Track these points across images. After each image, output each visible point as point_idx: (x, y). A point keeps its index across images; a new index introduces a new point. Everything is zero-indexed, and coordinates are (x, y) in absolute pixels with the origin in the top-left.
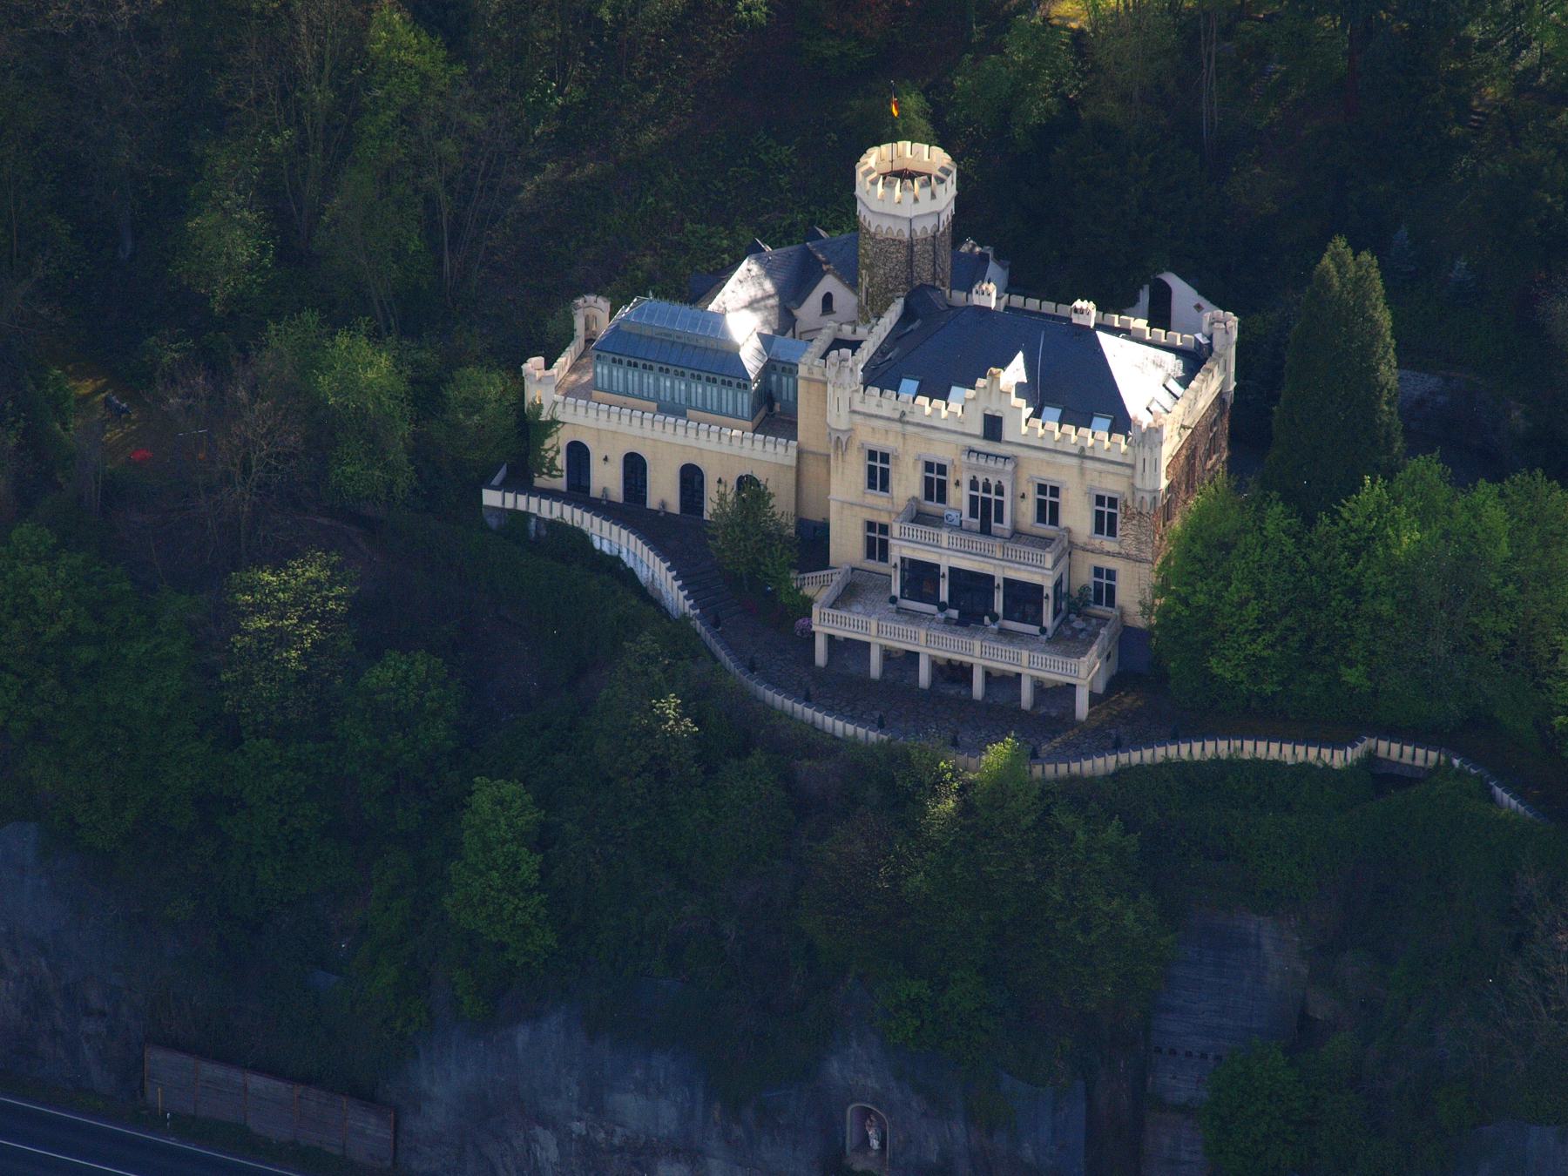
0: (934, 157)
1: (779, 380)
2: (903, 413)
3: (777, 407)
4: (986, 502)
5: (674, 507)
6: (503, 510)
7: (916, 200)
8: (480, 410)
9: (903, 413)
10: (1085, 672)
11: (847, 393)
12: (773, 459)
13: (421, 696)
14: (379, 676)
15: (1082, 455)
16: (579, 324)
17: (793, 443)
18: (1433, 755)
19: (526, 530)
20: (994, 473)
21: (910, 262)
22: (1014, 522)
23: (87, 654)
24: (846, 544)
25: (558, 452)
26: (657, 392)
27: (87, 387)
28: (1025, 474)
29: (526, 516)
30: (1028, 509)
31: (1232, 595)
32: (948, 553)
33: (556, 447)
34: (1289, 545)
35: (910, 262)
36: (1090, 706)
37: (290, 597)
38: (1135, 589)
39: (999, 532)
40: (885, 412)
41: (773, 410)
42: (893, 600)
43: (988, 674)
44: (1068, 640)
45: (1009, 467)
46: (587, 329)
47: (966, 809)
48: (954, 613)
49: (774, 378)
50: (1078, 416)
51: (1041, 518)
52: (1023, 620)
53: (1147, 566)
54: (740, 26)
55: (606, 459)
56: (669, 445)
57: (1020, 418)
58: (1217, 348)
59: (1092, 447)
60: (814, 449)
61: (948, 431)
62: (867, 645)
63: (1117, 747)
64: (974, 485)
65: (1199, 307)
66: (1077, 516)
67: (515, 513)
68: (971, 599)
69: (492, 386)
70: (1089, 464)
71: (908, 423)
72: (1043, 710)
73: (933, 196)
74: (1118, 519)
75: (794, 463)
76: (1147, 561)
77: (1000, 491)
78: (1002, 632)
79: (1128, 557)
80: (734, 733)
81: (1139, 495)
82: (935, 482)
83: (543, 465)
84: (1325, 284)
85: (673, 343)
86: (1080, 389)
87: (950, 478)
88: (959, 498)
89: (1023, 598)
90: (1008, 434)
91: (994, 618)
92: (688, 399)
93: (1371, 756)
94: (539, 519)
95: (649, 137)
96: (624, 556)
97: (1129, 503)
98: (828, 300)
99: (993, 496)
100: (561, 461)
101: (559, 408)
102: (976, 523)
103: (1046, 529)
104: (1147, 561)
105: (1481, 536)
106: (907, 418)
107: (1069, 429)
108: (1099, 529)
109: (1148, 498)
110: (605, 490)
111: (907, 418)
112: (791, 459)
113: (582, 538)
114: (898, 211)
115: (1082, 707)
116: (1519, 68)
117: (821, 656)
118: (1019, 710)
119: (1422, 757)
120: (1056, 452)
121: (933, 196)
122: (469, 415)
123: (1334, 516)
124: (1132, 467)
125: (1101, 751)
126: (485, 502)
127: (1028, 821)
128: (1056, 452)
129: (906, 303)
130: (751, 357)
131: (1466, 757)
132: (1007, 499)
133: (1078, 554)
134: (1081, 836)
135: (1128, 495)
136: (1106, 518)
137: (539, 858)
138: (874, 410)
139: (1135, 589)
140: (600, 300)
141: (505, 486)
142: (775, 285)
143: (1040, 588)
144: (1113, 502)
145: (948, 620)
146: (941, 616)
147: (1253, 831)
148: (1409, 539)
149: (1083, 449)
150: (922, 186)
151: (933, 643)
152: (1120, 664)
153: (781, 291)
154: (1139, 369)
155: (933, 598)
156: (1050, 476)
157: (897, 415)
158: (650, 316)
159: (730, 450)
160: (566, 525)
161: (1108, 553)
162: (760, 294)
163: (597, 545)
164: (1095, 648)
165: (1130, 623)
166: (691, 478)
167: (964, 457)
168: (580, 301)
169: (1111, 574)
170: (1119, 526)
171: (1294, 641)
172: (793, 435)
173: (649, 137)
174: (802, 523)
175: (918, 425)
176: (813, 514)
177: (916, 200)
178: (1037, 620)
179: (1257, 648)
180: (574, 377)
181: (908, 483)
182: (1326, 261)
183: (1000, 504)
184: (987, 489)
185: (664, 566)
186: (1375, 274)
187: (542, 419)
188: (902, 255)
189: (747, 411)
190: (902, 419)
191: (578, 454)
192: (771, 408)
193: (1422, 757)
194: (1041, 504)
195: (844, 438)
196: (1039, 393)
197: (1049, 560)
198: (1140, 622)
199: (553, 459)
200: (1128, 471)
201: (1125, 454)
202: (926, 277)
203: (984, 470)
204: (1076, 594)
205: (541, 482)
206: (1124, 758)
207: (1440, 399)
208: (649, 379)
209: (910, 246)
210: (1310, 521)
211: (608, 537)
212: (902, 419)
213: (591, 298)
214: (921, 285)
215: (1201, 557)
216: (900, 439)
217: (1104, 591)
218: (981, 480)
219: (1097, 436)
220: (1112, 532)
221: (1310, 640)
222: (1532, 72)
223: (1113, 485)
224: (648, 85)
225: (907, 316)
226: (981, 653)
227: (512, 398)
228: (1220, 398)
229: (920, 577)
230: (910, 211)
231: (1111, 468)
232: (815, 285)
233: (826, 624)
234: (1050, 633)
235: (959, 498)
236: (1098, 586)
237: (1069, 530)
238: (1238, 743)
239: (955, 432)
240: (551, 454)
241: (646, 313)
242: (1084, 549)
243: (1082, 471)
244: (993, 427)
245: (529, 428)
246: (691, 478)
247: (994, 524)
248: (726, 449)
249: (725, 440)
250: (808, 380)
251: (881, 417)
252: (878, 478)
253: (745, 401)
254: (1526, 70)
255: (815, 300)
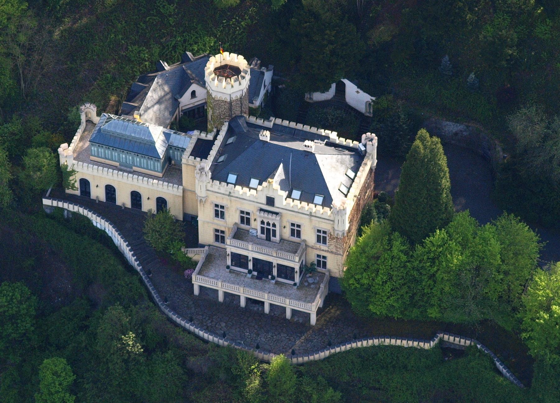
0: (239, 61)
1: (173, 153)
2: (230, 192)
3: (173, 162)
4: (268, 230)
5: (129, 205)
6: (52, 206)
7: (232, 86)
8: (40, 170)
9: (230, 192)
10: (312, 308)
11: (205, 184)
12: (172, 193)
13: (19, 307)
15: (311, 215)
16: (83, 118)
17: (181, 187)
18: (468, 342)
19: (63, 215)
20: (271, 219)
21: (230, 109)
22: (281, 236)
24: (206, 234)
25: (76, 181)
26: (119, 159)
29: (63, 209)
30: (287, 233)
31: (379, 280)
32: (251, 252)
33: (75, 180)
34: (404, 258)
35: (230, 109)
36: (317, 316)
38: (336, 265)
39: (274, 241)
40: (222, 191)
41: (171, 169)
42: (228, 267)
43: (271, 305)
44: (306, 288)
45: (278, 218)
46: (86, 116)
47: (264, 384)
48: (255, 273)
49: (171, 151)
50: (307, 197)
51: (293, 234)
52: (286, 278)
53: (340, 256)
55: (97, 186)
56: (125, 186)
58: (368, 151)
59: (315, 212)
60: (190, 189)
61: (251, 201)
63: (330, 345)
64: (262, 222)
65: (358, 92)
66: (309, 236)
67: (57, 208)
68: (262, 270)
69: (45, 157)
70: (313, 218)
71: (232, 196)
72: (296, 319)
73: (240, 84)
74: (327, 238)
75: (181, 195)
76: (340, 254)
77: (274, 225)
78: (277, 283)
79: (332, 252)
80: (158, 343)
81: (336, 232)
83: (70, 185)
84: (416, 151)
85: (125, 139)
86: (308, 182)
87: (252, 218)
90: (277, 203)
91: (273, 278)
92: (133, 162)
94: (68, 211)
97: (332, 234)
99: (271, 227)
100: (77, 185)
101: (75, 166)
102: (264, 236)
103: (295, 239)
104: (340, 254)
105: (488, 253)
106: (231, 195)
109: (340, 234)
110: (97, 197)
111: (231, 195)
112: (180, 192)
113: (89, 221)
114: (224, 91)
115: (313, 319)
117: (196, 291)
118: (285, 319)
119: (464, 342)
120: (299, 213)
122: (35, 172)
123: (422, 244)
124: (333, 221)
125: (323, 349)
126: (44, 203)
127: (292, 391)
128: (299, 213)
129: (229, 125)
130: (160, 149)
132: (277, 229)
133: (309, 250)
134: (315, 397)
135: (332, 231)
136: (322, 237)
137: (74, 397)
138: (217, 190)
139: (336, 265)
140: (92, 107)
142: (170, 87)
144: (325, 232)
145: (253, 277)
147: (391, 381)
149: (311, 213)
150: (235, 81)
152: (329, 290)
153: (172, 91)
154: (333, 167)
156: (297, 221)
157: (228, 193)
159: (152, 189)
160: (80, 215)
161: (323, 250)
162: (163, 94)
163: (95, 224)
164: (318, 296)
165: (333, 275)
166: (136, 197)
167: (258, 213)
169: (324, 257)
170: (327, 241)
171: (407, 297)
174: (185, 215)
175: (237, 197)
176: (190, 211)
177: (232, 86)
178: (293, 279)
181: (233, 218)
182: (418, 142)
183: (274, 231)
185: (125, 244)
186: (439, 145)
187: (68, 170)
188: (227, 106)
189: (159, 169)
190: (229, 195)
191: (85, 183)
192: (170, 163)
193: (464, 342)
194: (293, 231)
195: (204, 200)
196: (289, 185)
199: (73, 184)
200: (332, 223)
201: (330, 216)
202: (238, 113)
203: (267, 218)
204: (309, 266)
205: (69, 191)
207: (465, 133)
208: (115, 154)
209: (230, 103)
210: (413, 248)
211: (99, 222)
212: (229, 195)
213: (88, 105)
214: (235, 117)
215: (364, 261)
216: (229, 202)
217: (322, 262)
218: (266, 221)
220: (325, 242)
223: (324, 226)
225: (230, 132)
226: (268, 299)
229: (240, 260)
230: (229, 91)
231: (323, 220)
232: (188, 89)
234: (298, 285)
235: (256, 225)
236: (319, 262)
238: (383, 340)
239: (253, 202)
240: (73, 182)
241: (114, 123)
242: (312, 248)
244: (270, 201)
245: (61, 174)
246: (136, 197)
248: (151, 187)
249: (150, 184)
250: (187, 165)
251: (220, 193)
252: (219, 212)
253: (159, 165)
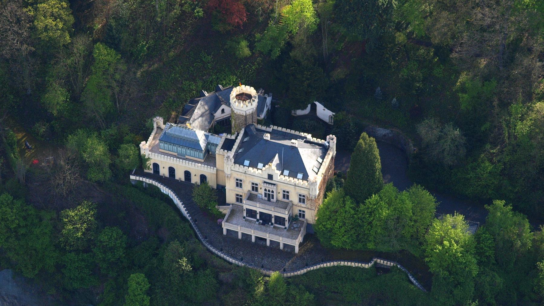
0: (251, 90)
3: (210, 153)
4: (269, 195)
14: (103, 238)
15: (295, 185)
16: (155, 126)
17: (215, 168)
18: (392, 264)
19: (142, 185)
21: (246, 120)
22: (277, 198)
23: (22, 231)
24: (230, 197)
27: (20, 136)
28: (279, 188)
29: (142, 182)
30: (280, 197)
31: (337, 225)
32: (258, 208)
33: (150, 164)
34: (353, 212)
35: (246, 120)
37: (78, 218)
38: (311, 216)
41: (209, 157)
42: (244, 218)
43: (271, 241)
45: (275, 187)
47: (266, 290)
50: (293, 175)
51: (284, 197)
52: (280, 224)
54: (196, 18)
56: (181, 167)
57: (277, 173)
58: (331, 146)
62: (238, 232)
63: (307, 265)
64: (265, 190)
65: (324, 110)
66: (294, 198)
67: (139, 181)
68: (265, 219)
69: (131, 150)
73: (252, 105)
78: (275, 227)
79: (308, 208)
82: (255, 187)
86: (293, 165)
87: (259, 187)
88: (261, 192)
89: (280, 220)
90: (274, 178)
91: (272, 224)
93: (376, 263)
94: (146, 183)
95: (171, 54)
96: (170, 195)
98: (223, 111)
99: (271, 193)
100: (151, 167)
102: (266, 199)
103: (286, 200)
107: (291, 179)
108: (300, 201)
109: (313, 197)
113: (159, 189)
114: (242, 109)
115: (297, 250)
116: (408, 31)
117: (225, 232)
118: (279, 249)
121: (252, 105)
122: (125, 159)
123: (364, 203)
125: (302, 268)
127: (284, 294)
130: (203, 144)
131: (402, 265)
132: (275, 194)
133: (294, 207)
134: (298, 297)
136: (302, 199)
137: (149, 298)
139: (311, 216)
141: (136, 174)
143: (284, 218)
144: (304, 196)
146: (257, 223)
148: (385, 213)
151: (254, 233)
153: (210, 109)
154: (309, 156)
155: (255, 217)
156: (287, 189)
158: (175, 131)
159: (197, 169)
162: (204, 111)
163: (162, 191)
164: (300, 235)
165: (309, 222)
166: (187, 174)
168: (155, 119)
169: (304, 212)
172: (215, 165)
173: (171, 54)
174: (218, 185)
176: (221, 183)
178: (284, 225)
179: (345, 239)
180: (154, 142)
181: (247, 187)
182: (361, 141)
183: (273, 195)
184: (269, 191)
186: (374, 142)
188: (244, 118)
189: (202, 157)
191: (156, 166)
192: (209, 153)
194: (284, 195)
196: (282, 167)
197: (287, 213)
198: (311, 223)
202: (250, 122)
206: (309, 269)
208: (175, 148)
209: (246, 116)
210: (358, 206)
211: (165, 190)
213: (158, 118)
215: (328, 214)
218: (267, 189)
219: (299, 181)
220: (304, 202)
221: (359, 234)
222: (412, 33)
223: (303, 192)
224: (171, 37)
226: (269, 237)
227: (137, 152)
228: (332, 157)
229: (251, 213)
230: (245, 109)
233: (226, 226)
235: (261, 192)
236: (300, 214)
237: (291, 201)
241: (174, 129)
243: (295, 188)
244: (270, 177)
245: (142, 160)
247: (271, 200)
252: (239, 184)
253: (202, 155)
254: (410, 32)
255: (220, 111)
